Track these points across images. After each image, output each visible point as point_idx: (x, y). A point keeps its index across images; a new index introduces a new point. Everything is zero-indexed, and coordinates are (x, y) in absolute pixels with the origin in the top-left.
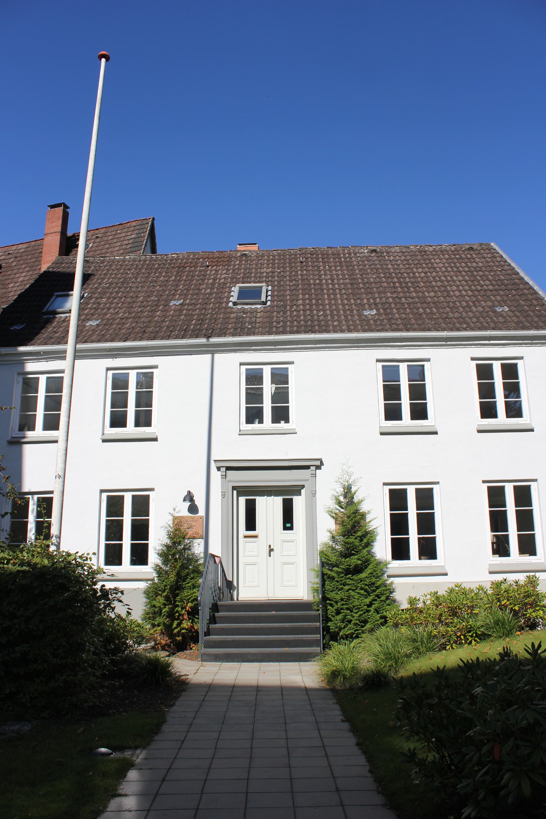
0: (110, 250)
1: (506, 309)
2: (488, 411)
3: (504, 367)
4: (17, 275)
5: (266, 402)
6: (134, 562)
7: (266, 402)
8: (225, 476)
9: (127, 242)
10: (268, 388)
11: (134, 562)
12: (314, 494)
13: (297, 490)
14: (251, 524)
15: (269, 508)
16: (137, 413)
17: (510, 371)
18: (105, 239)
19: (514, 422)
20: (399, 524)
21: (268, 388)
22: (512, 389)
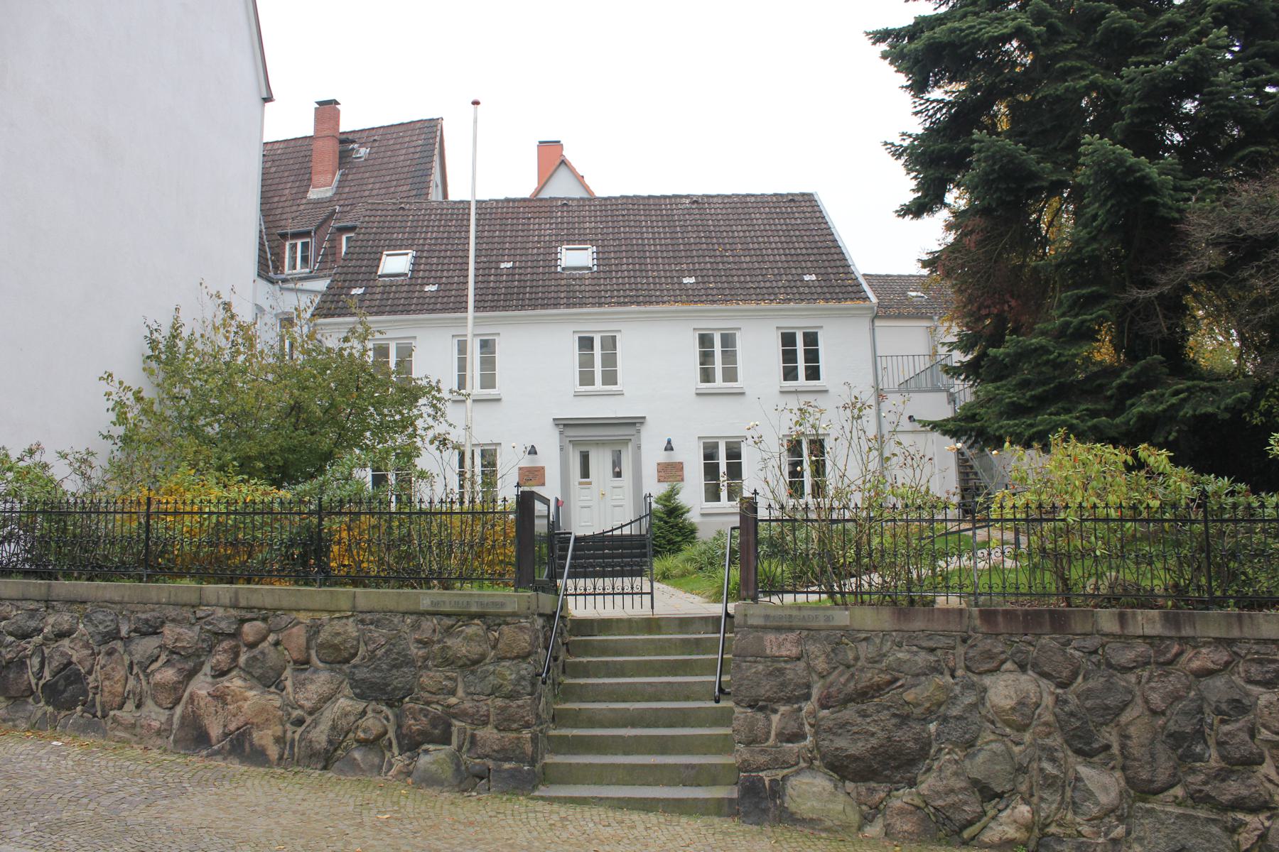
0: (393, 160)
1: (814, 277)
2: (790, 374)
3: (806, 335)
4: (280, 187)
5: (597, 361)
6: (808, 378)
7: (597, 361)
8: (561, 433)
9: (412, 150)
10: (801, 364)
11: (808, 378)
12: (639, 448)
13: (626, 442)
14: (585, 473)
15: (600, 462)
16: (807, 368)
17: (811, 339)
18: (385, 143)
19: (813, 384)
20: (711, 471)
21: (801, 364)
22: (812, 356)
